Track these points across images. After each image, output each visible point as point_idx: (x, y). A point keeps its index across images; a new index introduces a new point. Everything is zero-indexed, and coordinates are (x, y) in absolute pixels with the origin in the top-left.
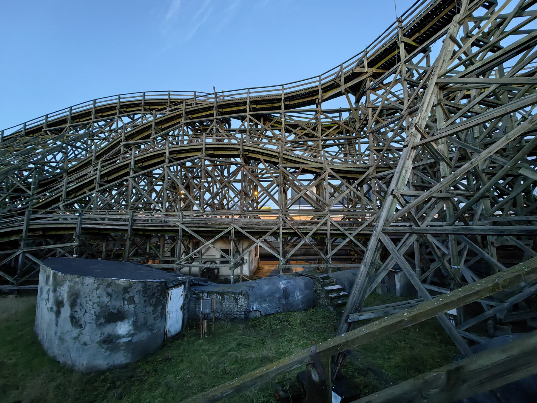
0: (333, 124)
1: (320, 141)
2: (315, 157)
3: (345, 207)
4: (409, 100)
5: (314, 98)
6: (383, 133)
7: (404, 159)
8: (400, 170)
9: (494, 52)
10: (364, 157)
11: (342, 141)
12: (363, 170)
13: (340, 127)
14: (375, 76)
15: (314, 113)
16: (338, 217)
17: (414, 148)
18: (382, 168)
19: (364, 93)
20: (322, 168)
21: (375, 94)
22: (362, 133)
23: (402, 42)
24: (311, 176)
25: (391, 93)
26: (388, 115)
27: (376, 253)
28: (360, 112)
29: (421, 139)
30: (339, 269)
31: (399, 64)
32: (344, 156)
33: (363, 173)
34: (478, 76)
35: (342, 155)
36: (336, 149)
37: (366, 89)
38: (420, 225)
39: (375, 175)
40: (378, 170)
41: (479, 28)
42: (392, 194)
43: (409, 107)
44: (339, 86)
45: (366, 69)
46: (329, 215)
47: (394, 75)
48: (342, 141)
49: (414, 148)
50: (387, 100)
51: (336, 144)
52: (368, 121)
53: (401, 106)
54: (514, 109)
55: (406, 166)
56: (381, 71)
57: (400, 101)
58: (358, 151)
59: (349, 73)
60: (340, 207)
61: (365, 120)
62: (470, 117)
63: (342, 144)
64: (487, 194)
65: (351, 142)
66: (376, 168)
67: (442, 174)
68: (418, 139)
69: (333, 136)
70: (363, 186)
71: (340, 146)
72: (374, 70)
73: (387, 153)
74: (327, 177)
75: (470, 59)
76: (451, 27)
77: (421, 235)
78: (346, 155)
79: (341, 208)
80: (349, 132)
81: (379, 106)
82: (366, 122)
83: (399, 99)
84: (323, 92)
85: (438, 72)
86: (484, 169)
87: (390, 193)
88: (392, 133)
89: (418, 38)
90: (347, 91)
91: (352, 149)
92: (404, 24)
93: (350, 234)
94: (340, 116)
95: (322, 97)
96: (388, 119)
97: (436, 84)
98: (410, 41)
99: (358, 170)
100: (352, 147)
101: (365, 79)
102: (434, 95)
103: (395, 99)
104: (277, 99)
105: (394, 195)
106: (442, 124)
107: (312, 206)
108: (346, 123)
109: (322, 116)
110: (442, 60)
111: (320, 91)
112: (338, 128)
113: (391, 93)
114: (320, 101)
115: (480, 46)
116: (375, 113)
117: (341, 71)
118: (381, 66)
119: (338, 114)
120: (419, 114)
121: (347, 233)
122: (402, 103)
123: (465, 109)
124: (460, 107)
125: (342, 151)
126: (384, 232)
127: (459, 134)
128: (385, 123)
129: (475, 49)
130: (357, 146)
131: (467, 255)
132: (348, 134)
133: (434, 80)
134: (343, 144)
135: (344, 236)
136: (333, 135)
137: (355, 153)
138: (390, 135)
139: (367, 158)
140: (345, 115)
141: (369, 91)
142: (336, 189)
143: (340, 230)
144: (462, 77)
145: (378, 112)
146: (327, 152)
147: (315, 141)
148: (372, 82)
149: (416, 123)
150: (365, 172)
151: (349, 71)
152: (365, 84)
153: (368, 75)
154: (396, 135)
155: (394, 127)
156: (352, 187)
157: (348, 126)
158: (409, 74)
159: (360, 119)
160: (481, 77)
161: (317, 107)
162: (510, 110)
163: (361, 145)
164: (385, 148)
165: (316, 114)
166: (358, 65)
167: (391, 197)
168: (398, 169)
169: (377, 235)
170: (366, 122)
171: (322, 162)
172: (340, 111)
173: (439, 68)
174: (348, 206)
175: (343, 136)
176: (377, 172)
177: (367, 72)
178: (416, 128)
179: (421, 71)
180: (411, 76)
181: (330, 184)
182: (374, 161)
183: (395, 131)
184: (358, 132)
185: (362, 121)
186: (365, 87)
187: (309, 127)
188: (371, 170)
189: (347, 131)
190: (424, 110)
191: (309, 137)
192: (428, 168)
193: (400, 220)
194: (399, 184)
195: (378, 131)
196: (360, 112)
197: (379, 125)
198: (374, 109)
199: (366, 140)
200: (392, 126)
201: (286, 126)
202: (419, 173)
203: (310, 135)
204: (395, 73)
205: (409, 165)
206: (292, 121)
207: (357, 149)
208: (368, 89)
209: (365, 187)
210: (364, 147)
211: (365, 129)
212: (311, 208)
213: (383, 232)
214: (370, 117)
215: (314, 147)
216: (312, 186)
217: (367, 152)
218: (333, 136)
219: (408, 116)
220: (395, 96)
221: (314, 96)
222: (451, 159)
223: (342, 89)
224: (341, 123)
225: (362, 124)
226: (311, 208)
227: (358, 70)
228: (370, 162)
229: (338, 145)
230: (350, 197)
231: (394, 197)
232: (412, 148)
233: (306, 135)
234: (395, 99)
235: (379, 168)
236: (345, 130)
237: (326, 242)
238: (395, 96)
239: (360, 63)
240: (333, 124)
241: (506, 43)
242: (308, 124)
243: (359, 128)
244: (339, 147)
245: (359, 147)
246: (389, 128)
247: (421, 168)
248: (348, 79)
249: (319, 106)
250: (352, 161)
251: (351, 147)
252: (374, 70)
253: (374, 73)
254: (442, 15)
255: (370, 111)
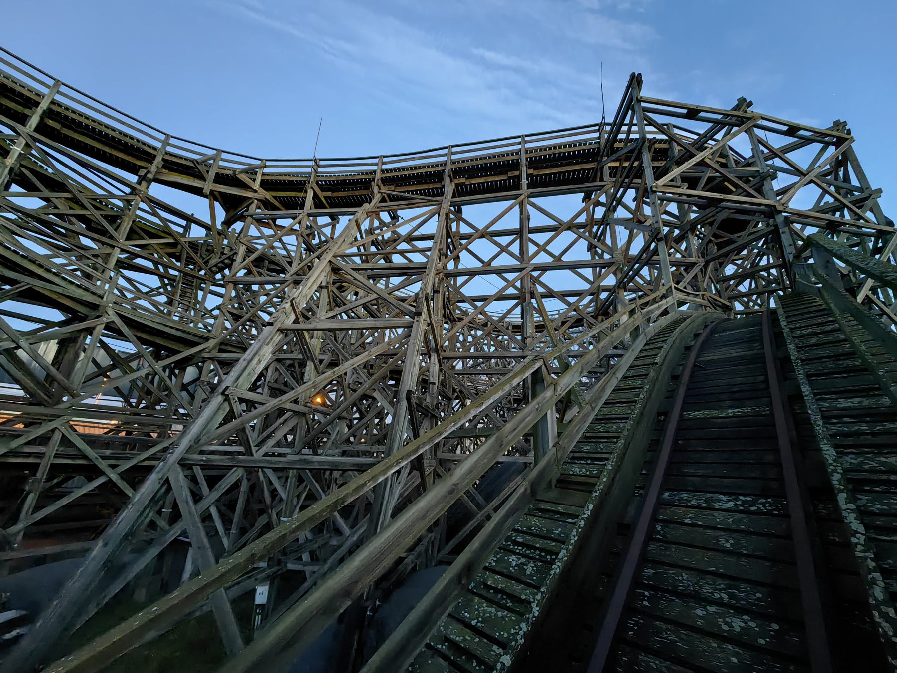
0: (164, 232)
1: (117, 250)
2: (88, 276)
3: (130, 404)
4: (299, 264)
5: (138, 163)
6: (254, 291)
7: (262, 341)
8: (250, 357)
9: (386, 262)
10: (207, 318)
11: (172, 272)
12: (196, 339)
13: (179, 247)
14: (266, 204)
15: (128, 190)
16: (99, 427)
17: (280, 330)
18: (231, 346)
19: (242, 218)
20: (94, 307)
21: (258, 230)
22: (218, 276)
23: (312, 188)
24: (56, 315)
25: (281, 241)
26: (269, 270)
27: (149, 508)
28: (225, 242)
29: (294, 322)
30: (40, 561)
31: (301, 211)
32: (166, 303)
33: (193, 344)
34: (369, 277)
35: (163, 299)
36: (154, 281)
37: (247, 213)
38: (254, 452)
39: (215, 354)
40: (223, 347)
41: (381, 230)
42: (223, 393)
43: (297, 274)
44: (202, 178)
45: (256, 186)
46: (69, 418)
47: (290, 221)
48: (172, 272)
49: (280, 330)
50: (273, 248)
51: (157, 272)
52: (234, 263)
53: (287, 266)
54: (382, 325)
55: (261, 353)
56: (276, 204)
57: (289, 260)
58: (199, 302)
59: (228, 172)
60: (117, 403)
61: (229, 258)
62: (353, 317)
63: (172, 279)
64: (345, 414)
65: (191, 282)
66: (221, 344)
67: (306, 378)
68: (289, 321)
69: (156, 255)
70: (184, 370)
71: (166, 281)
72: (268, 196)
73: (251, 326)
74: (100, 329)
75: (366, 255)
76: (361, 212)
77: (251, 471)
78: (170, 302)
79: (119, 405)
80: (194, 263)
81: (258, 249)
82: (230, 262)
83: (289, 256)
84: (164, 167)
85: (335, 249)
86: (350, 384)
87: (221, 391)
88: (265, 297)
89: (330, 197)
90: (213, 196)
91: (188, 295)
92: (320, 170)
93: (113, 467)
94: (187, 229)
95: (157, 173)
96: (268, 275)
97: (330, 261)
98: (321, 195)
99: (184, 336)
100: (190, 291)
101: (251, 198)
102: (324, 274)
103: (284, 252)
104: (29, 99)
105: (227, 395)
106: (323, 313)
107: (24, 388)
108: (193, 245)
109: (143, 205)
110: (342, 239)
111: (158, 161)
112: (174, 245)
113: (281, 241)
114: (150, 176)
115: (378, 249)
116: (249, 257)
117: (214, 158)
118: (279, 197)
119: (184, 223)
120: (301, 287)
121: (103, 465)
122: (290, 263)
123: (349, 306)
124: (345, 301)
125: (166, 289)
126: (184, 464)
127: (338, 332)
128: (259, 278)
129: (373, 249)
130: (200, 294)
131: (306, 499)
132: (191, 267)
133: (328, 257)
134: (174, 278)
135: (92, 471)
136: (158, 253)
137: (191, 303)
138: (263, 299)
139: (211, 321)
140: (197, 232)
141: (249, 219)
142: (119, 361)
143: (85, 457)
144: (353, 269)
145: (253, 257)
146: (129, 280)
147: (103, 243)
148: (260, 211)
149: (294, 298)
150: (199, 344)
151: (229, 169)
152: (248, 207)
153: (256, 196)
154: (270, 302)
155: (271, 290)
156: (159, 366)
157: (196, 253)
158: (308, 232)
159: (222, 253)
160: (371, 281)
161: (139, 183)
162: (378, 325)
163: (209, 295)
164: (246, 316)
165: (131, 194)
166: (245, 172)
167: (220, 398)
168: (247, 355)
169: (166, 469)
170: (230, 262)
171: (100, 292)
172: (190, 220)
173: (337, 246)
174: (139, 403)
175: (178, 264)
176: (221, 351)
177: (256, 191)
178: (292, 305)
179: (323, 239)
180: (311, 237)
181: (104, 346)
182: (222, 330)
183: (270, 297)
184: (212, 271)
185: (224, 257)
186: (247, 211)
187: (97, 208)
188: (211, 343)
189: (190, 260)
190: (309, 285)
191: (89, 228)
192: (296, 365)
193: (233, 441)
194: (241, 380)
195: (247, 286)
196: (225, 242)
197: (250, 278)
198: (250, 251)
199: (222, 290)
200: (268, 287)
201: (23, 169)
202: (282, 370)
203: (93, 225)
204: (294, 218)
205: (267, 354)
206: (50, 171)
207: (200, 298)
208: (251, 216)
209: (191, 372)
210: (212, 302)
211: (227, 271)
212: (21, 393)
213: (180, 464)
214: (239, 258)
215: (94, 256)
216: (48, 338)
217: (216, 312)
218: (156, 255)
219: (292, 285)
220: (285, 249)
221: (141, 159)
222: (321, 361)
223: (208, 187)
224: (183, 240)
225: (222, 262)
226: (21, 393)
227: (243, 177)
228: (215, 329)
229: (161, 277)
230: (149, 386)
231: (225, 400)
232: (278, 330)
233: (81, 218)
234: (284, 252)
235: (226, 345)
236: (187, 257)
237: (27, 488)
238: (285, 249)
239: (251, 172)
240: (164, 232)
241: (397, 259)
242: (98, 202)
243: (216, 266)
244: (162, 282)
245: (204, 297)
246: (264, 289)
247: (288, 362)
248: (220, 179)
249: (144, 184)
250: (181, 317)
251: (187, 290)
252: (268, 196)
253: (266, 199)
254: (357, 193)
255: (242, 250)
